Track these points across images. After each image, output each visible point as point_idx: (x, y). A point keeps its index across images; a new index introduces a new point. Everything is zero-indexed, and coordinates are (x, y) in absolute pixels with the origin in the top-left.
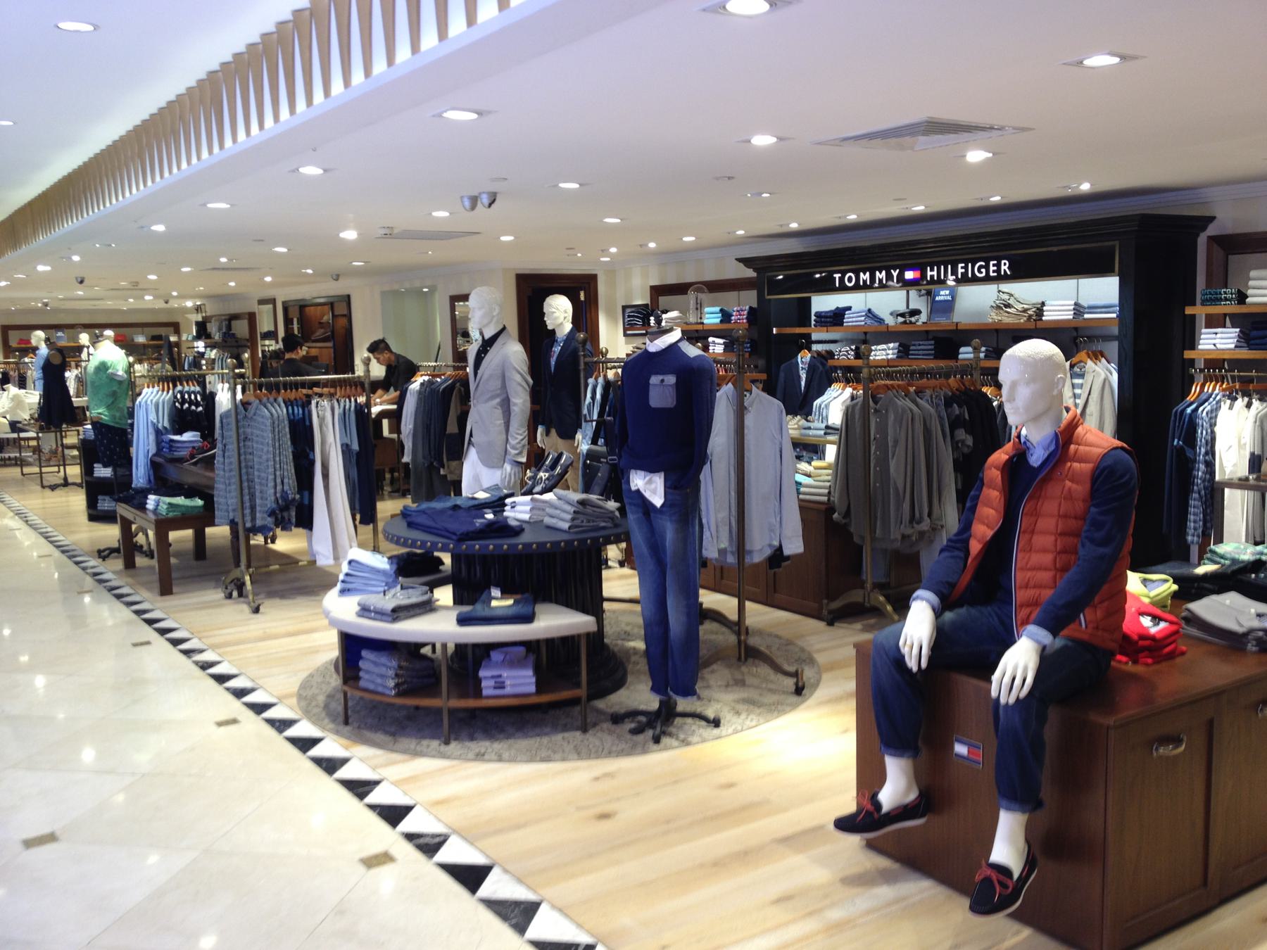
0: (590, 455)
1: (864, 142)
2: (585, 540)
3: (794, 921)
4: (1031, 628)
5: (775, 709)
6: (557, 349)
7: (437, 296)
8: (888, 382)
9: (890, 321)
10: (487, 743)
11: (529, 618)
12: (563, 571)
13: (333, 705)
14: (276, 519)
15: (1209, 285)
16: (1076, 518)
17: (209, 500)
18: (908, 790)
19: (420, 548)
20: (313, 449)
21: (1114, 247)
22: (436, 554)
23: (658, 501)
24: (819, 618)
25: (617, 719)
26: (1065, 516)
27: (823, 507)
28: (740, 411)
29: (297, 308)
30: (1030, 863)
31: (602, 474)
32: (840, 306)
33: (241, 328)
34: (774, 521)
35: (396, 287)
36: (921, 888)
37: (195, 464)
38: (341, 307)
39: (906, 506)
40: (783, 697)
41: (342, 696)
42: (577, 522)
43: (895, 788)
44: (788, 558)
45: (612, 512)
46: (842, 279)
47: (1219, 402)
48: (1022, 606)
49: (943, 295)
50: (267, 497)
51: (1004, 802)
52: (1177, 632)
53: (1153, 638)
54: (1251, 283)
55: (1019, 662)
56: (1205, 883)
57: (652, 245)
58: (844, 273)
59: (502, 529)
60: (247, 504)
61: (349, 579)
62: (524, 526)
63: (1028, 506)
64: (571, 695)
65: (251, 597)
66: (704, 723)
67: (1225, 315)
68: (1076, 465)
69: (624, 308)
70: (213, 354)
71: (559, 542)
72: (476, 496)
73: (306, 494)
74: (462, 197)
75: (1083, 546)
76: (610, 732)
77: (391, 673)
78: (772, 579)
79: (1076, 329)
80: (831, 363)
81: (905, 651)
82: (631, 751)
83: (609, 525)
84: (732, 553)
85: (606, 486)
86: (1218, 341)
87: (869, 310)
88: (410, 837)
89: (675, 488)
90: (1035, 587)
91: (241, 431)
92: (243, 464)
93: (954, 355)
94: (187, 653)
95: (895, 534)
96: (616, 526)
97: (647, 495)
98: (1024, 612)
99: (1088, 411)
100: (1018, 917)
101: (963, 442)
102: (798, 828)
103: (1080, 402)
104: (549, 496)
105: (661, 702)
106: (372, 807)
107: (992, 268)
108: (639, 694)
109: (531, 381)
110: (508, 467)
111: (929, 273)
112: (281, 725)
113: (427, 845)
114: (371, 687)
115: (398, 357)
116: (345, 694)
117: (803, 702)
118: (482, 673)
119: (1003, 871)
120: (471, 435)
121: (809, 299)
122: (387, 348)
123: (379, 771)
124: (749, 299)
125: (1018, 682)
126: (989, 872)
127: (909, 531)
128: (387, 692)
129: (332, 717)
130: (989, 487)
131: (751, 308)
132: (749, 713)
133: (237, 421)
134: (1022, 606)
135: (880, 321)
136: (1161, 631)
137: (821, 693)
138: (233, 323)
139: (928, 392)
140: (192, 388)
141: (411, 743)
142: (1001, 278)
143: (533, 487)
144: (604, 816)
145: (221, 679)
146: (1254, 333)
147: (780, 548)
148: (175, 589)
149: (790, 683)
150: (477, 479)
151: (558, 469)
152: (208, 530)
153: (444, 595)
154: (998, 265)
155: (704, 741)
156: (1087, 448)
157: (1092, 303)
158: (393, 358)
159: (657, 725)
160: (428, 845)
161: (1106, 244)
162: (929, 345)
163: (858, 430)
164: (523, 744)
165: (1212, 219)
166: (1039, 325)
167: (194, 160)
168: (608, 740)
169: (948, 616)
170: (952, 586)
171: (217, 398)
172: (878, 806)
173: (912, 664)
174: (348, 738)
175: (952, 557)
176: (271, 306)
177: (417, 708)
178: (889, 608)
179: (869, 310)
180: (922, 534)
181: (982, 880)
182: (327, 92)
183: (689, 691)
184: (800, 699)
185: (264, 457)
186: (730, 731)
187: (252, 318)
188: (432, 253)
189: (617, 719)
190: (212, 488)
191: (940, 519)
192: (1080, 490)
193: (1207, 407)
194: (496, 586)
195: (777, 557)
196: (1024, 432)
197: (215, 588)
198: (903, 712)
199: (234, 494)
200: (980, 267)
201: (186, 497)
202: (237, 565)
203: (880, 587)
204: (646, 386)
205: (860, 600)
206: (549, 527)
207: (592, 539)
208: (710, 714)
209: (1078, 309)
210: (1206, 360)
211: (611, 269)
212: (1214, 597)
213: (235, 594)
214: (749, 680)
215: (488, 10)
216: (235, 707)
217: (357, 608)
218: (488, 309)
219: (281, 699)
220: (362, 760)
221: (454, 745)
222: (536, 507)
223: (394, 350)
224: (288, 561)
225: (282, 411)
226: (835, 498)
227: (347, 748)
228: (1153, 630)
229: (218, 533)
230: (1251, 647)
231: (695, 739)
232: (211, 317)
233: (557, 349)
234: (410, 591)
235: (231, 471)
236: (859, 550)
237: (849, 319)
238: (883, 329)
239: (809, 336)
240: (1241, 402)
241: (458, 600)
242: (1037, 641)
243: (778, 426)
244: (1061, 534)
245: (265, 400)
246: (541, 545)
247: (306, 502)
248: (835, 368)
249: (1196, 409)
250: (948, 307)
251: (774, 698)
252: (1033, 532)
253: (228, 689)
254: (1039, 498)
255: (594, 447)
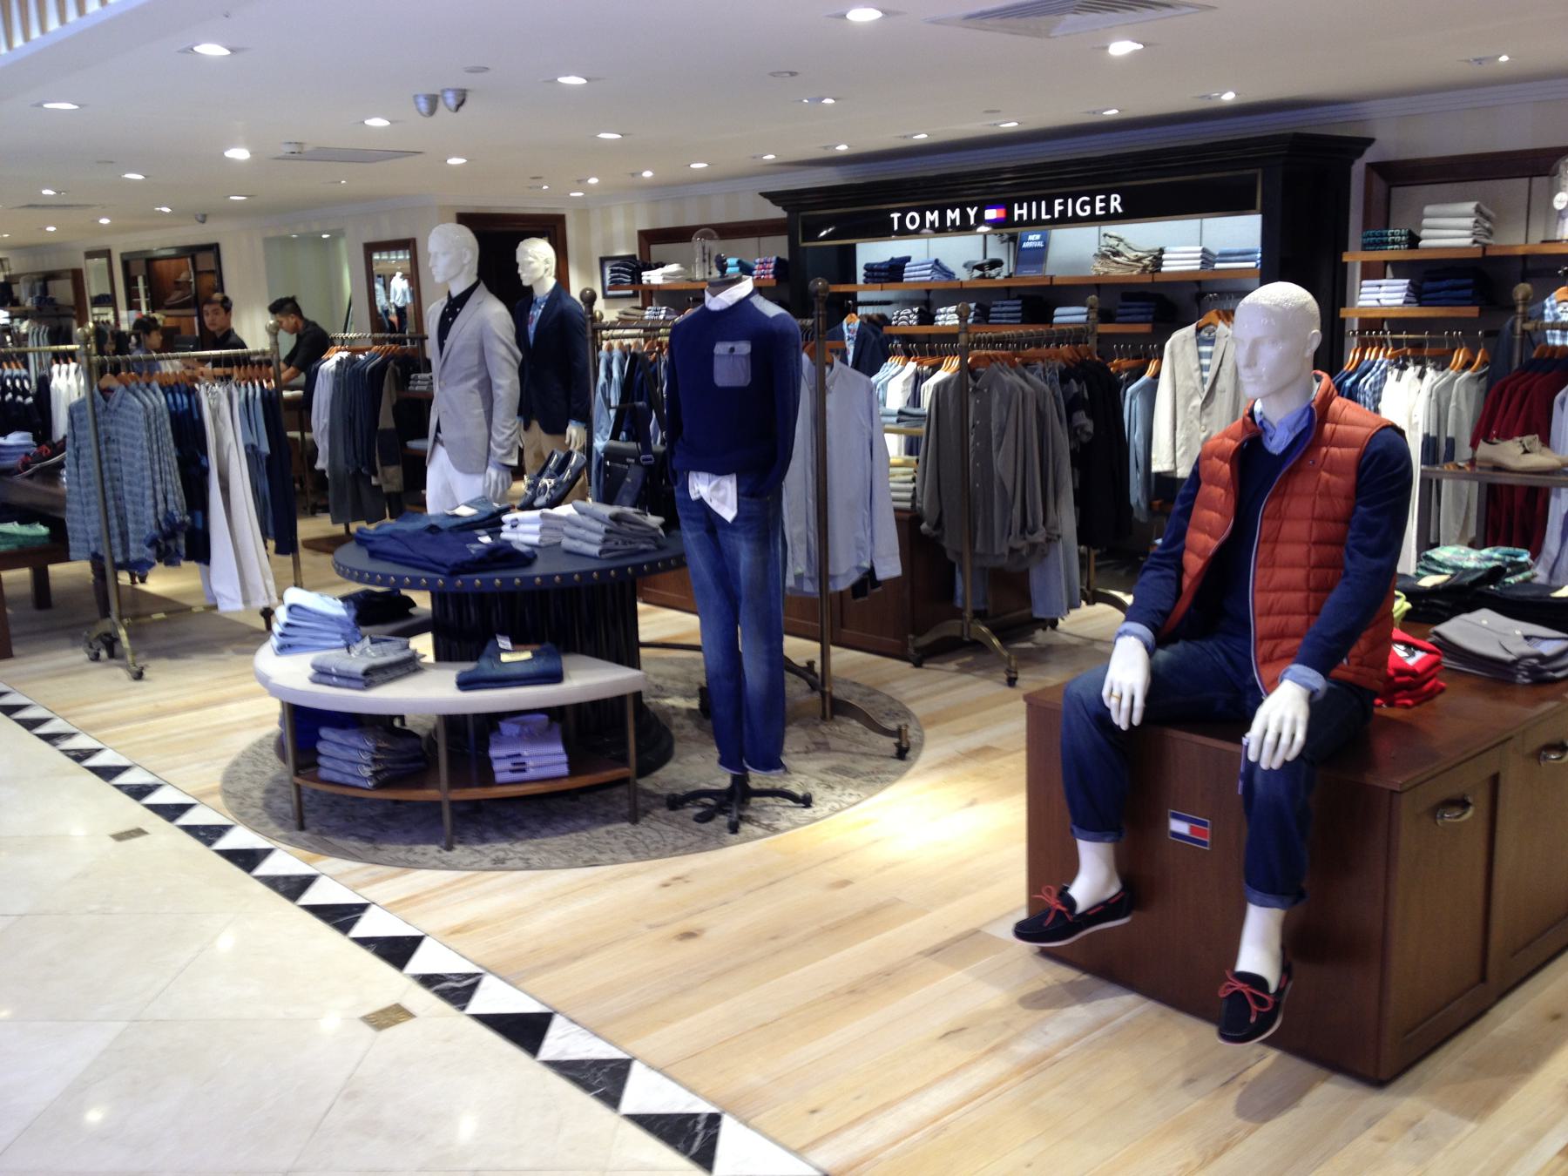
0: (609, 453)
1: (1013, 21)
2: (625, 568)
3: (973, 1062)
4: (1297, 668)
5: (877, 780)
6: (536, 313)
7: (343, 245)
8: (990, 352)
9: (963, 275)
10: (505, 845)
11: (556, 677)
12: (586, 612)
13: (277, 803)
14: (159, 550)
15: (1366, 225)
16: (1335, 521)
17: (59, 531)
18: (1107, 886)
19: (380, 584)
20: (205, 452)
21: (1256, 175)
22: (404, 592)
23: (728, 513)
24: (903, 657)
25: (675, 802)
26: (1321, 519)
27: (907, 516)
28: (821, 392)
29: (143, 263)
30: (1286, 970)
31: (633, 478)
32: (897, 255)
33: (62, 291)
34: (863, 535)
35: (285, 232)
36: (1123, 1005)
37: (30, 477)
38: (204, 258)
39: (1016, 512)
40: (883, 762)
41: (293, 790)
42: (610, 545)
43: (1090, 882)
44: (879, 583)
45: (655, 530)
46: (902, 220)
47: (1386, 370)
48: (1262, 639)
49: (1033, 240)
50: (144, 520)
51: (1258, 895)
52: (1437, 663)
53: (1411, 672)
54: (1426, 222)
55: (1282, 715)
56: (1483, 978)
57: (647, 174)
58: (904, 212)
59: (507, 556)
60: (116, 531)
61: (290, 631)
62: (537, 551)
63: (1270, 506)
64: (606, 779)
65: (129, 658)
66: (790, 803)
67: (1386, 263)
68: (1334, 450)
69: (603, 261)
70: (24, 327)
71: (572, 575)
72: (457, 512)
73: (199, 514)
74: (416, 97)
75: (1351, 556)
76: (670, 822)
77: (366, 757)
78: (856, 613)
79: (1199, 283)
80: (887, 330)
81: (1111, 703)
82: (702, 845)
83: (652, 547)
84: (811, 579)
85: (639, 494)
86: (1383, 296)
87: (937, 261)
88: (428, 981)
89: (752, 495)
90: (1280, 613)
91: (101, 428)
92: (106, 475)
93: (1047, 318)
94: (49, 738)
95: (1001, 547)
96: (660, 548)
97: (714, 505)
98: (1266, 647)
99: (1218, 386)
100: (1271, 1043)
101: (1082, 427)
102: (948, 936)
103: (1209, 375)
104: (565, 510)
105: (734, 778)
106: (364, 942)
107: (1098, 205)
108: (699, 767)
109: (520, 355)
110: (493, 472)
111: (1017, 212)
112: (206, 835)
113: (454, 989)
114: (337, 777)
115: (307, 323)
116: (298, 787)
117: (909, 767)
118: (493, 753)
119: (1256, 981)
120: (438, 429)
121: (853, 247)
122: (297, 311)
123: (362, 891)
124: (778, 247)
125: (1285, 740)
126: (1239, 986)
127: (1019, 544)
128: (361, 784)
129: (280, 820)
130: (1210, 483)
131: (778, 259)
132: (845, 785)
133: (95, 416)
134: (1262, 639)
135: (950, 275)
136: (1419, 662)
137: (928, 755)
138: (51, 284)
139: (1040, 364)
140: (16, 372)
141: (400, 851)
142: (1110, 217)
143: (534, 498)
144: (689, 935)
145: (107, 773)
146: (1427, 285)
147: (871, 572)
148: (15, 650)
149: (889, 743)
150: (448, 489)
151: (567, 475)
152: (54, 569)
153: (423, 645)
154: (1107, 201)
155: (796, 825)
156: (1349, 428)
157: (1226, 249)
158: (301, 325)
159: (729, 810)
160: (457, 991)
161: (1246, 172)
162: (1014, 306)
163: (952, 414)
164: (556, 842)
165: (1369, 141)
166: (1158, 278)
167: (35, 33)
168: (670, 832)
169: (1162, 654)
170: (1165, 615)
171: (53, 385)
172: (1071, 903)
173: (1121, 721)
174: (308, 848)
175: (1163, 577)
176: (104, 261)
177: (397, 802)
178: (995, 641)
179: (937, 261)
180: (1034, 546)
181: (1230, 997)
182: (43, 29)
183: (772, 762)
184: (903, 763)
185: (137, 465)
186: (826, 810)
187: (77, 276)
188: (346, 180)
189: (675, 802)
190: (63, 508)
191: (1055, 527)
192: (1342, 483)
193: (1370, 378)
194: (503, 634)
195: (868, 579)
196: (1258, 407)
197: (74, 646)
198: (1092, 779)
199: (95, 517)
200: (1083, 204)
201: (21, 523)
202: (105, 612)
203: (980, 615)
204: (709, 357)
205: (958, 633)
206: (569, 552)
207: (633, 566)
208: (794, 787)
209: (1207, 258)
210: (1362, 320)
211: (584, 208)
212: (1465, 616)
213: (104, 654)
214: (834, 742)
215: (93, 6)
216: (135, 813)
217: (311, 671)
218: (451, 256)
219: (201, 796)
220: (336, 880)
221: (459, 850)
222: (548, 525)
223: (307, 314)
224: (173, 608)
225: (159, 400)
226: (924, 504)
227: (308, 862)
228: (1411, 662)
229: (70, 572)
230: (1523, 678)
231: (782, 824)
232: (18, 276)
233: (536, 313)
234: (385, 645)
235: (88, 484)
236: (953, 565)
237: (910, 273)
238: (955, 285)
239: (853, 296)
240: (1412, 371)
241: (444, 654)
242: (1305, 685)
243: (867, 412)
244: (1315, 543)
245: (133, 385)
246: (566, 577)
247: (199, 525)
248: (891, 337)
249: (1357, 382)
250: (1040, 255)
251: (874, 763)
252: (1276, 541)
253: (119, 787)
254: (1284, 495)
255: (614, 443)
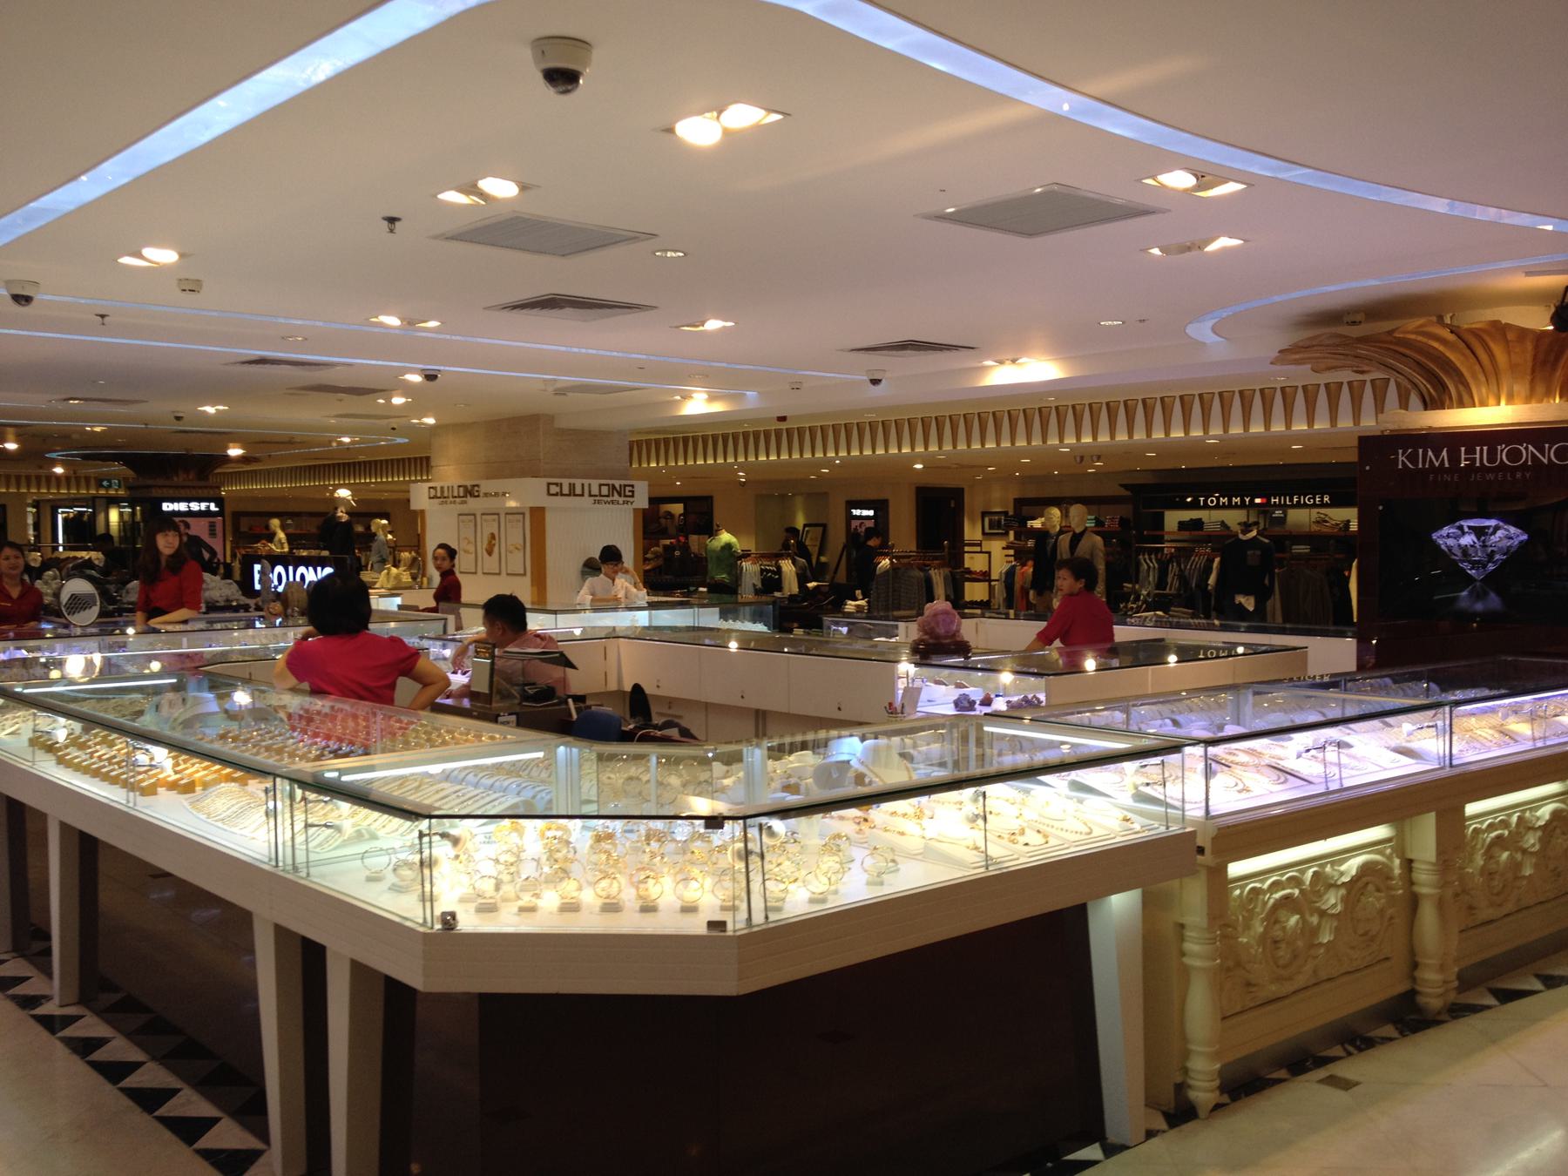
49: (1278, 513)
69: (984, 514)
142: (1323, 505)
250: (1282, 521)
